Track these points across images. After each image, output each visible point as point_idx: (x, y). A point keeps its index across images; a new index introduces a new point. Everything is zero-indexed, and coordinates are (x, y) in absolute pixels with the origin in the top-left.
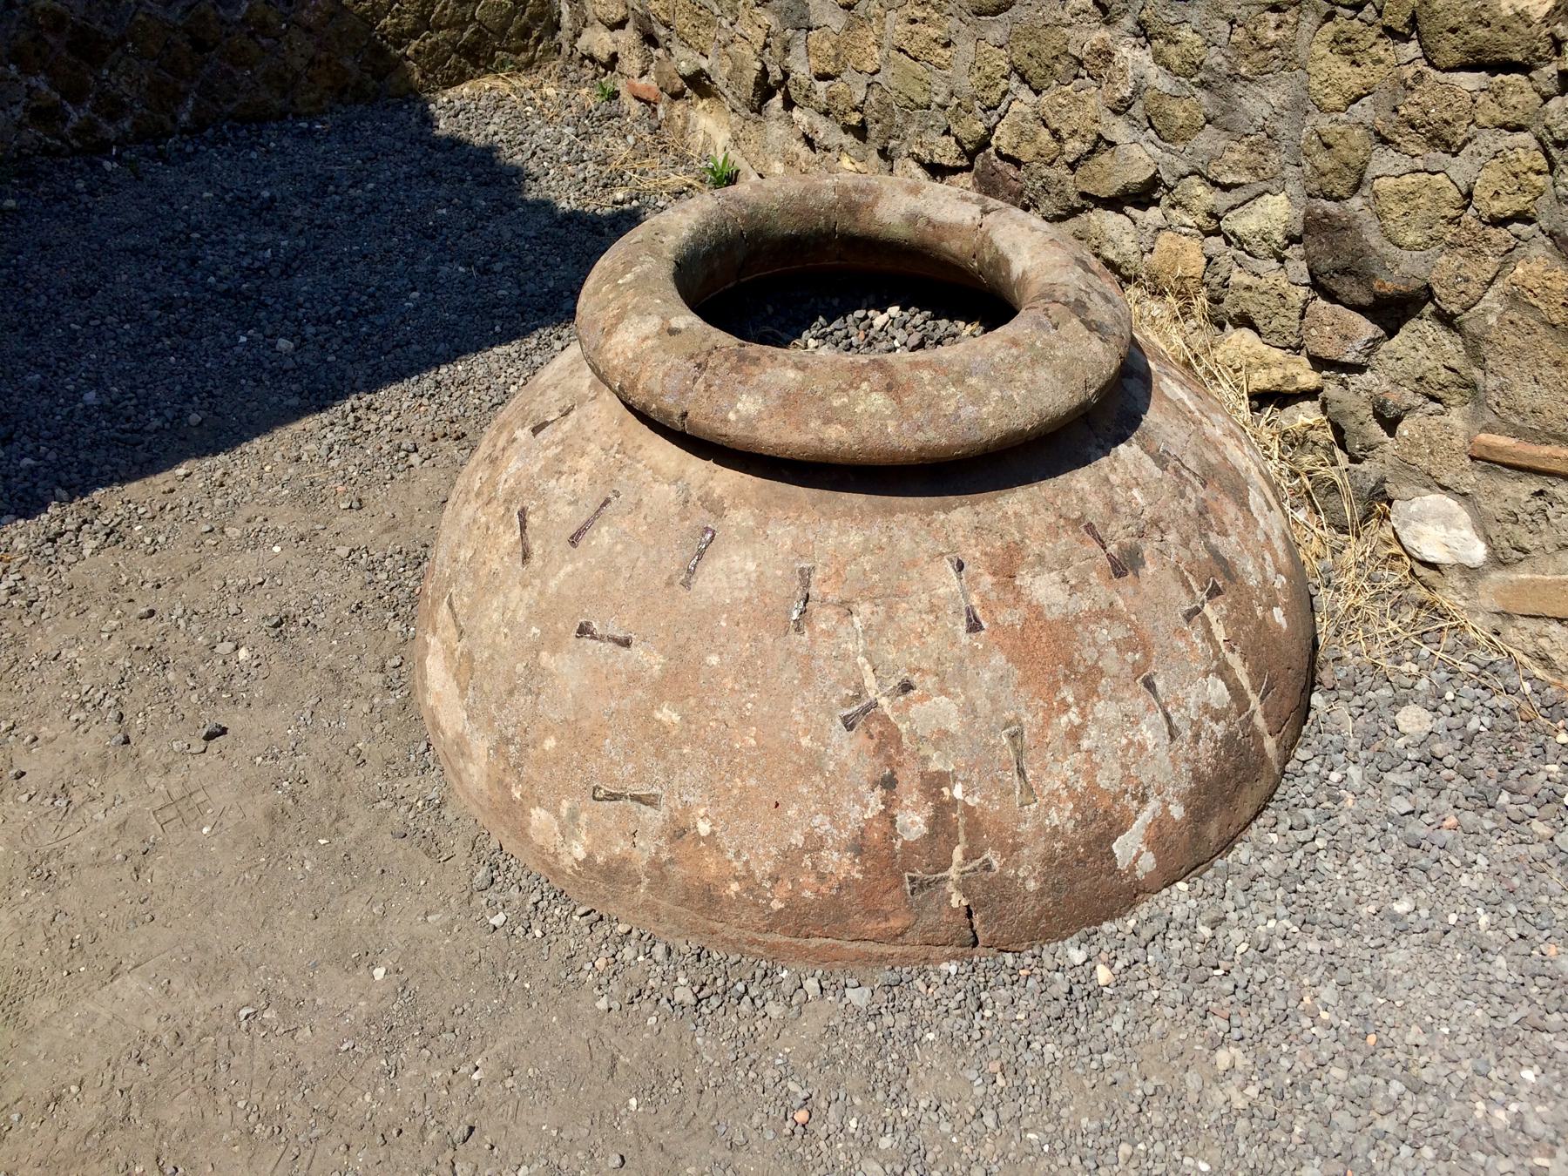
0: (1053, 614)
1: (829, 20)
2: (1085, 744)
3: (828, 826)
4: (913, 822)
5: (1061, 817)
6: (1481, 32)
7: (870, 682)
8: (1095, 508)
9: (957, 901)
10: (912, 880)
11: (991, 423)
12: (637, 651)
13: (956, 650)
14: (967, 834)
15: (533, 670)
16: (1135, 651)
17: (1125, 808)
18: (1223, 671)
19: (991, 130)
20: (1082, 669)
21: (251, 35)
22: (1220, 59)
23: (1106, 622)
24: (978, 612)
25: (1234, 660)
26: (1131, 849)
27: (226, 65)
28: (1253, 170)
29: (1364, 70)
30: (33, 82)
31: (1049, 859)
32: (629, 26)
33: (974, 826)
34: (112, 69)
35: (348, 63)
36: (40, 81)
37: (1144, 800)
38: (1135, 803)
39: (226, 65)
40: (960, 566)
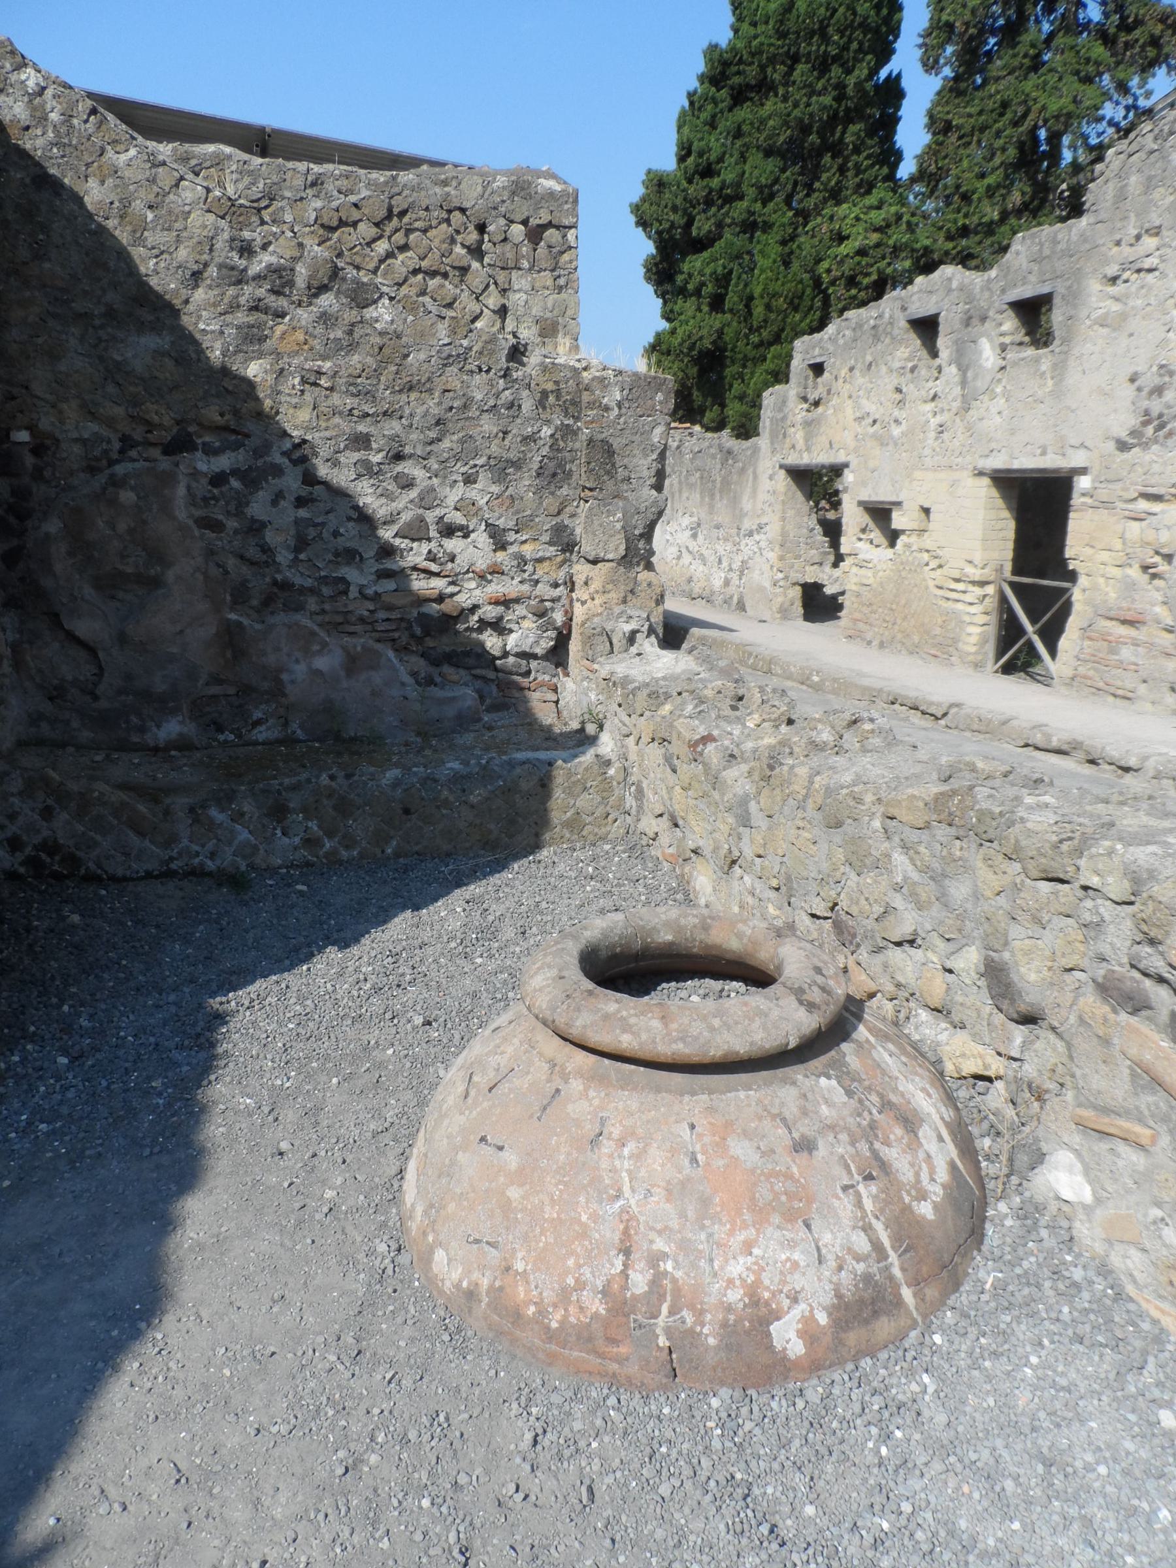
2: (756, 1251)
4: (639, 1282)
5: (735, 1296)
6: (1043, 860)
8: (791, 1110)
9: (663, 1341)
10: (635, 1321)
12: (504, 1154)
14: (672, 1295)
15: (453, 1163)
18: (867, 1229)
21: (438, 807)
25: (879, 1226)
26: (787, 1335)
28: (960, 931)
31: (724, 1325)
32: (665, 817)
33: (677, 1291)
35: (492, 826)
36: (313, 825)
37: (795, 1300)
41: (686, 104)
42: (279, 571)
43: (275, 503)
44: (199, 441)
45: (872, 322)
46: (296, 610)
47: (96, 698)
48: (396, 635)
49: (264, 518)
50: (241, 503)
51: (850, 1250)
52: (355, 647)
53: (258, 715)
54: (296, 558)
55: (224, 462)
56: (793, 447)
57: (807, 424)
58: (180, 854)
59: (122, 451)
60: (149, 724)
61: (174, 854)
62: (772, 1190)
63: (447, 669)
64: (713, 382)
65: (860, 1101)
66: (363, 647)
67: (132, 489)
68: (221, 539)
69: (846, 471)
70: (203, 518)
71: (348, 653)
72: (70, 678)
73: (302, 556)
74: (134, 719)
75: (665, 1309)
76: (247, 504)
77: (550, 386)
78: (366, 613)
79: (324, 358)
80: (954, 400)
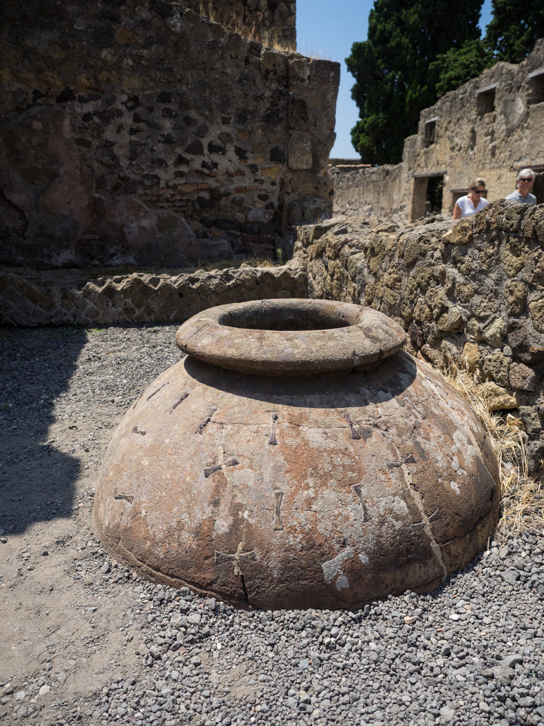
0: (315, 445)
1: (370, 280)
2: (314, 507)
3: (187, 520)
4: (223, 525)
7: (221, 457)
11: (298, 356)
13: (262, 450)
16: (354, 472)
17: (331, 548)
18: (406, 497)
19: (412, 311)
20: (321, 472)
22: (476, 264)
23: (341, 455)
24: (277, 436)
27: (189, 302)
29: (521, 257)
30: (127, 301)
34: (152, 299)
36: (129, 301)
37: (344, 544)
38: (338, 546)
39: (189, 302)
40: (276, 418)
41: (374, 8)
42: (121, 171)
43: (118, 131)
44: (76, 95)
45: (461, 96)
46: (132, 193)
47: (25, 238)
48: (186, 209)
49: (113, 140)
50: (100, 131)
51: (391, 511)
52: (163, 214)
53: (111, 251)
54: (131, 163)
55: (89, 107)
56: (419, 165)
57: (426, 153)
58: (56, 314)
59: (34, 100)
60: (53, 253)
61: (53, 314)
62: (331, 463)
63: (214, 229)
64: (382, 144)
65: (409, 408)
66: (168, 215)
67: (40, 120)
68: (90, 152)
69: (445, 175)
70: (79, 139)
71: (160, 218)
72: (11, 227)
73: (134, 163)
74: (45, 251)
75: (240, 547)
76: (103, 132)
77: (270, 67)
78: (169, 196)
79: (144, 48)
80: (502, 132)
